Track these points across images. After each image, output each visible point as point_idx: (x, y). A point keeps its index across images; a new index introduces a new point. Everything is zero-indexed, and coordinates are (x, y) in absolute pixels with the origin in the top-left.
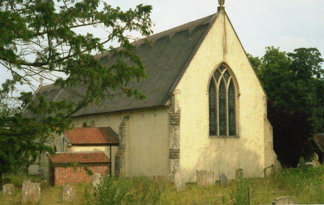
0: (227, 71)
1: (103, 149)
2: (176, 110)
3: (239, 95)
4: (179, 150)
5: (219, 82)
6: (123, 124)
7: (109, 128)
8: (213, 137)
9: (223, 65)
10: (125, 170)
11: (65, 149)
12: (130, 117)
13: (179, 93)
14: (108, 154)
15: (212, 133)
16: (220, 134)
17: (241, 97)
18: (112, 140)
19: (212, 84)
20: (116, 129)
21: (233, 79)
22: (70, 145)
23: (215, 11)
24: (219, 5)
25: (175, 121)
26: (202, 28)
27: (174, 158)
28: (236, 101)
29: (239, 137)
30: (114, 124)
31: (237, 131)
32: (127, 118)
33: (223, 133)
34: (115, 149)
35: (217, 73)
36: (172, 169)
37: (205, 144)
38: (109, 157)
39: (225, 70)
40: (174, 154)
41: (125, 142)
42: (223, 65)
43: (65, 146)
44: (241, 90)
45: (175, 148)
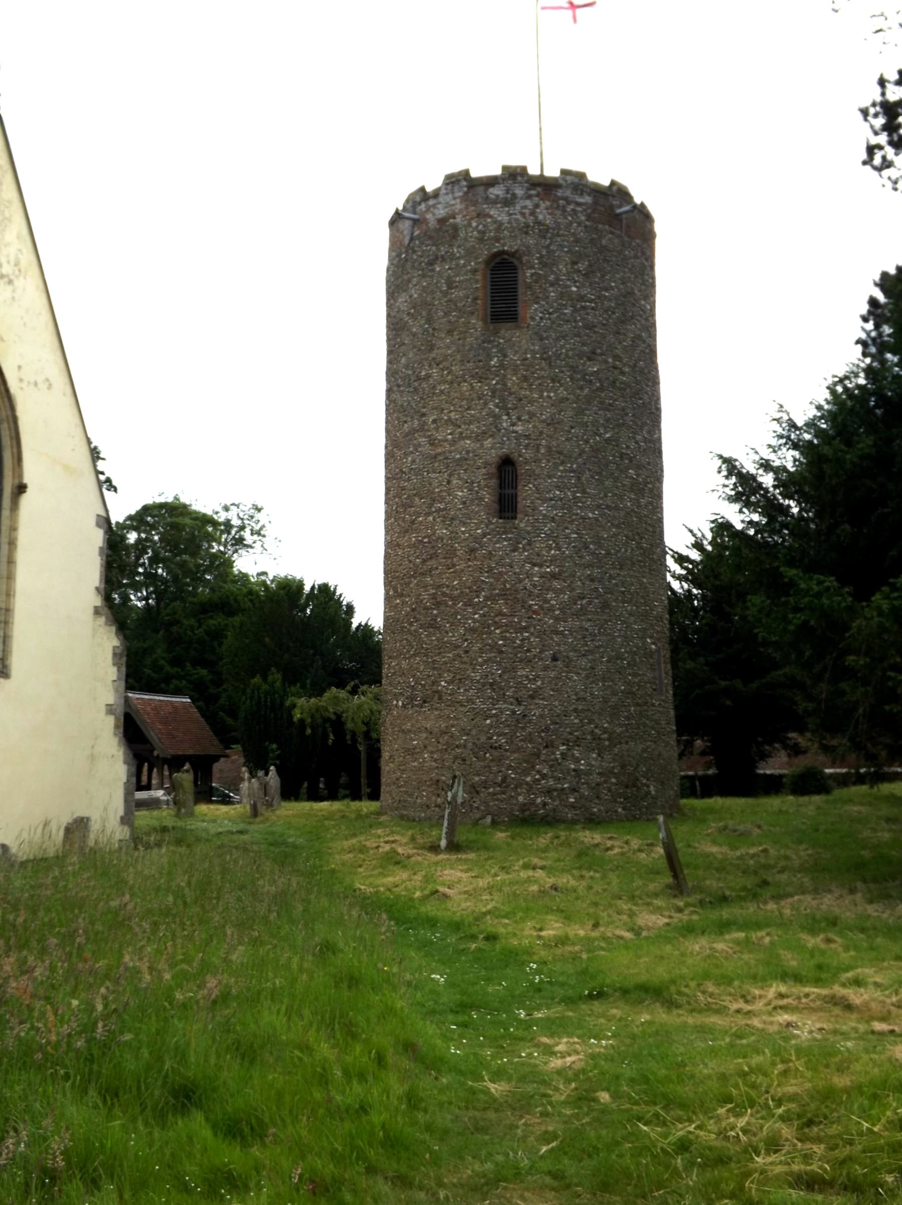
3: (21, 488)
17: (26, 501)
44: (31, 472)
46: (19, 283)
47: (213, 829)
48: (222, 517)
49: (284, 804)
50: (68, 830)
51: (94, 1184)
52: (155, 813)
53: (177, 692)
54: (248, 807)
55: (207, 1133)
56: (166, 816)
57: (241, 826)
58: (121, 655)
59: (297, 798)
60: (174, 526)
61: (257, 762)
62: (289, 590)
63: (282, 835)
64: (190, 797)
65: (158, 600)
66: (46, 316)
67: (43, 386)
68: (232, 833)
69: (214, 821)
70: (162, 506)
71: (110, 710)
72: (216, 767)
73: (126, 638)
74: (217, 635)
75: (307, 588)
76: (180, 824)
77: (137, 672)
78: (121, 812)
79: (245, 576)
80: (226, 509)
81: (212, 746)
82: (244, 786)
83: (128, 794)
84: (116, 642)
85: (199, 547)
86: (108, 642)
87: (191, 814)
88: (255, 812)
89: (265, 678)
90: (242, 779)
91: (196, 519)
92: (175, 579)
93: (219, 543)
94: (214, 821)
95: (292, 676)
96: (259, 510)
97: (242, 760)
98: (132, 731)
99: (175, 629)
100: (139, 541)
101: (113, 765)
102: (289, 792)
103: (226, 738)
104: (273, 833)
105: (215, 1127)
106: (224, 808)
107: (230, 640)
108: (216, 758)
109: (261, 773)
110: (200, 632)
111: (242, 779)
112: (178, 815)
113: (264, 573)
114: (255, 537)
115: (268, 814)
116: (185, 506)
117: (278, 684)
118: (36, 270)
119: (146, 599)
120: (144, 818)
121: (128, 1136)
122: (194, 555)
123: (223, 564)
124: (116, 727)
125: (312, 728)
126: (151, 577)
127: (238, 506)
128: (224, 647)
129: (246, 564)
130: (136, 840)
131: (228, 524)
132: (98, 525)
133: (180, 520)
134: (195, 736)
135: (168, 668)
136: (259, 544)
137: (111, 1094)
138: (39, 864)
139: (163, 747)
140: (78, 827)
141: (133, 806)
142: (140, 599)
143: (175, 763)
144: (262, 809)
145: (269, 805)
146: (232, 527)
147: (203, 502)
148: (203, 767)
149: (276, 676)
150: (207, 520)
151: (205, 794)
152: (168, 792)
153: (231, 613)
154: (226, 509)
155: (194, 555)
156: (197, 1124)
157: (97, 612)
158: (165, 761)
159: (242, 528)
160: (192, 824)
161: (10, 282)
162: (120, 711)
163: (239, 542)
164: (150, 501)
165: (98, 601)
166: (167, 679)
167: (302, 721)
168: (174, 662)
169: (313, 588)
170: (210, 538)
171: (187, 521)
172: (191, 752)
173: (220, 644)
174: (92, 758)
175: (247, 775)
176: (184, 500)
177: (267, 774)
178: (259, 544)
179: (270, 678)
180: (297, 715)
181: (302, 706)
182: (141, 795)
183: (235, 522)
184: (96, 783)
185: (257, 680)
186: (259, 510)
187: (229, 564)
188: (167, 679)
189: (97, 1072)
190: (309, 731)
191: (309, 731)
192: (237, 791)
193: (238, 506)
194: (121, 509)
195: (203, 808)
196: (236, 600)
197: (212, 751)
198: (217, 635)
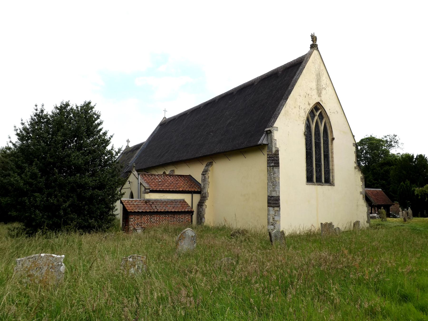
0: (321, 113)
1: (187, 198)
2: (274, 150)
3: (333, 139)
4: (279, 197)
5: (314, 124)
6: (204, 173)
7: (190, 176)
8: (309, 183)
9: (318, 107)
10: (209, 219)
11: (143, 195)
12: (214, 163)
13: (277, 130)
14: (189, 203)
15: (309, 180)
16: (317, 181)
17: (334, 141)
18: (197, 188)
19: (308, 127)
20: (198, 177)
21: (327, 122)
22: (147, 191)
23: (308, 49)
24: (312, 43)
25: (274, 161)
26: (294, 68)
27: (274, 207)
28: (330, 146)
29: (334, 186)
30: (195, 171)
31: (331, 178)
32: (211, 164)
33: (319, 181)
34: (197, 198)
35: (312, 113)
36: (271, 220)
37: (116, 210)
38: (191, 206)
39: (319, 111)
40: (274, 202)
41: (210, 190)
42: (318, 107)
43: (142, 192)
44: (335, 135)
45: (274, 194)
46: (327, 89)
47: (392, 225)
48: (385, 139)
49: (414, 218)
50: (354, 224)
51: (384, 317)
52: (375, 220)
53: (377, 187)
54: (403, 219)
55: (413, 309)
56: (378, 221)
57: (402, 224)
58: (363, 179)
59: (418, 217)
60: (372, 144)
61: (404, 206)
62: (408, 158)
63: (415, 227)
64: (385, 216)
65: (368, 164)
66: (335, 95)
67: (336, 113)
68: (399, 226)
69: (393, 223)
70: (367, 138)
71: (361, 193)
72: (391, 207)
73: (364, 174)
74: (387, 172)
75: (415, 157)
76: (382, 223)
77: (368, 183)
78: (366, 220)
79: (394, 154)
80: (386, 137)
81: (388, 201)
82: (401, 213)
83: (368, 215)
84: (361, 175)
85: (379, 148)
86: (359, 175)
87: (386, 221)
88: (405, 220)
89: (404, 183)
90: (400, 211)
91: (377, 141)
92: (373, 157)
93: (385, 146)
94: (393, 223)
95: (413, 182)
96: (396, 136)
97: (399, 206)
98: (367, 199)
99: (375, 171)
100: (361, 148)
101: (363, 208)
102: (415, 215)
103: (393, 200)
104: (412, 226)
105: (416, 308)
106: (395, 219)
107: (392, 172)
108: (391, 205)
109: (406, 209)
110: (382, 171)
111: (400, 211)
112: (382, 221)
113: (399, 153)
114: (395, 144)
115: (409, 221)
116: (374, 138)
117: (409, 184)
118: (331, 85)
119: (365, 163)
120: (372, 221)
121: (394, 308)
122: (377, 150)
123: (386, 152)
124: (363, 197)
125: (421, 196)
126: (366, 158)
127: (389, 136)
128: (390, 175)
129: (393, 151)
130: (371, 226)
131: (387, 141)
132: (353, 146)
133: (373, 142)
134: (384, 199)
135: (373, 181)
136: (396, 146)
137: (384, 294)
138: (348, 232)
139: (375, 202)
140: (357, 224)
141: (370, 218)
142: (363, 164)
143: (379, 207)
144: (407, 219)
145: (409, 218)
146: (388, 142)
147: (379, 136)
148: (387, 207)
149: (408, 182)
150: (380, 141)
151: (389, 215)
152: (378, 214)
153: (390, 166)
154: (386, 137)
155: (377, 150)
156: (410, 306)
157: (355, 168)
158: (376, 206)
159: (391, 141)
160: (384, 223)
161: (325, 89)
162: (364, 193)
163: (391, 145)
164: (363, 138)
165: (355, 165)
166: (374, 184)
167: (417, 195)
168: (375, 180)
169: (417, 156)
170: (382, 145)
171: (374, 141)
172: (383, 204)
173: (389, 174)
174: (357, 206)
175: (401, 210)
176: (373, 136)
177: (408, 210)
178: (396, 146)
179: (406, 183)
180: (416, 193)
181: (417, 190)
182: (371, 215)
183: (389, 140)
184: (359, 212)
185: (402, 183)
186: (396, 136)
187: (389, 152)
188: (374, 184)
189: (379, 288)
190: (420, 197)
191: (420, 197)
192: (398, 214)
193: (389, 136)
194: (358, 140)
195: (389, 219)
196: (392, 162)
197: (389, 203)
198: (387, 172)
